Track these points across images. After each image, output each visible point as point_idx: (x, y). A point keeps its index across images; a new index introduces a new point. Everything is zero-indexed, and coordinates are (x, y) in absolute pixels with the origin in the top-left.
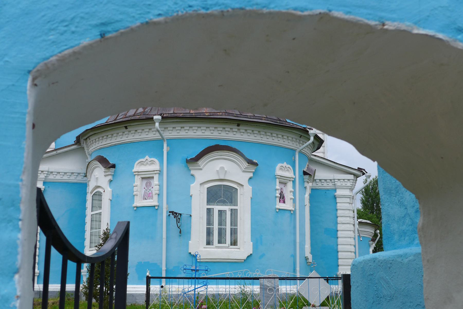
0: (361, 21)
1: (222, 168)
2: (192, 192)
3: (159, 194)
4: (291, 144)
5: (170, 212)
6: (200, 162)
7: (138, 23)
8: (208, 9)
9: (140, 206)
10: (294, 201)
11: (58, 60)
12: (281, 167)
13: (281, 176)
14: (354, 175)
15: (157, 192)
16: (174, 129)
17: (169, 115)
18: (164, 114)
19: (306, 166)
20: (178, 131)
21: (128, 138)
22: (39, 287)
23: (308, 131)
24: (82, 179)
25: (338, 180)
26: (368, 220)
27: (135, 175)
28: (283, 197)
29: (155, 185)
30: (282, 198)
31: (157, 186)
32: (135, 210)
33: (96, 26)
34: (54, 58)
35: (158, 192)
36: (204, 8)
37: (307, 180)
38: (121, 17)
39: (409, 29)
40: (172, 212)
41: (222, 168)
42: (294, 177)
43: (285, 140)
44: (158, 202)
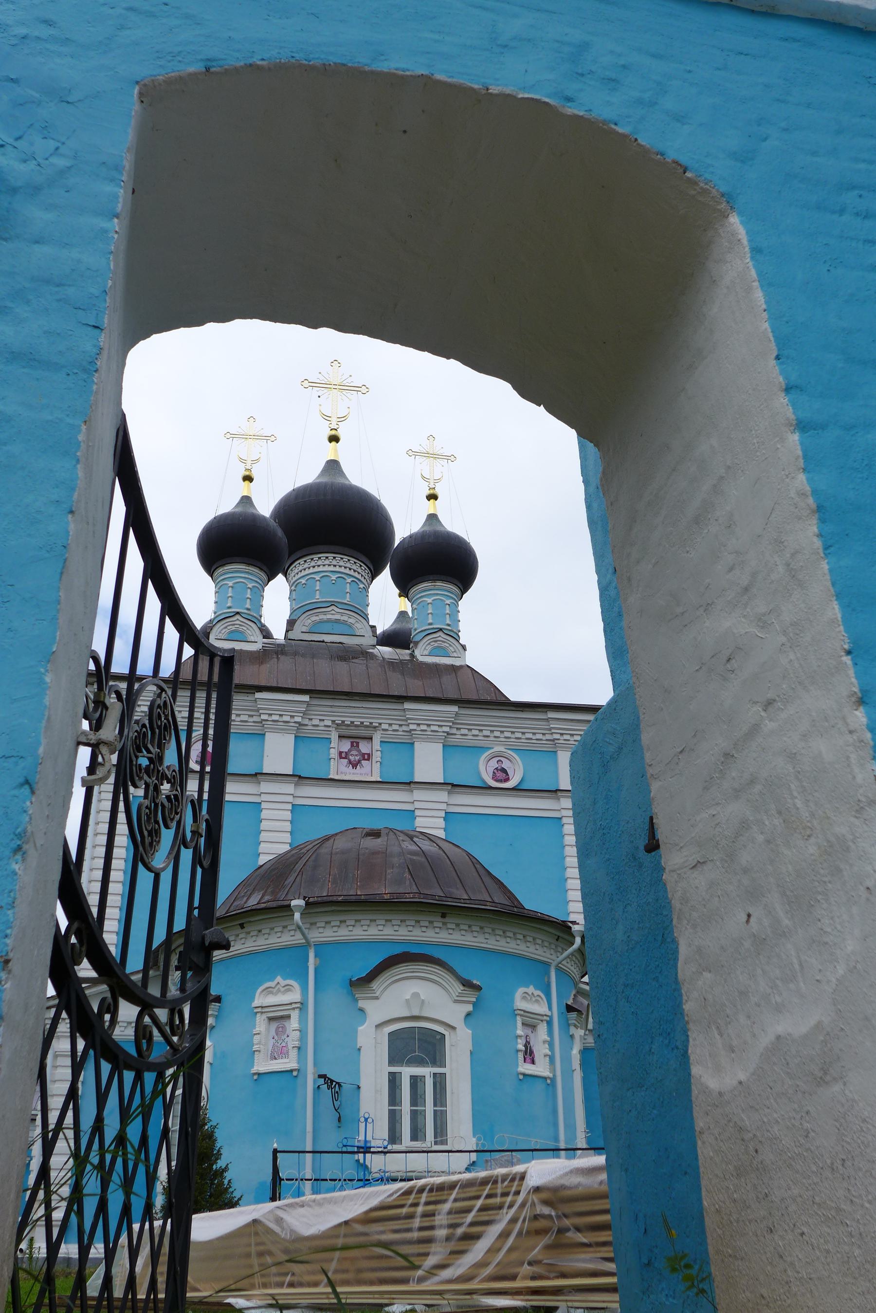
0: (464, 84)
1: (416, 995)
2: (361, 1041)
3: (299, 1048)
4: (540, 952)
5: (320, 1076)
6: (375, 985)
7: (242, 63)
8: (310, 61)
9: (264, 1071)
10: (552, 1059)
11: (164, 81)
12: (523, 995)
13: (525, 1011)
15: (297, 1043)
16: (328, 925)
17: (319, 899)
18: (309, 898)
19: (570, 996)
20: (335, 929)
21: (246, 946)
22: (67, 1249)
23: (570, 928)
27: (256, 1013)
28: (532, 1053)
29: (293, 1030)
30: (529, 1055)
31: (297, 1031)
32: (256, 1080)
33: (202, 60)
34: (161, 77)
35: (297, 1043)
36: (306, 60)
37: (574, 1022)
38: (224, 57)
39: (514, 93)
41: (416, 995)
42: (550, 1015)
43: (528, 944)
44: (298, 1063)
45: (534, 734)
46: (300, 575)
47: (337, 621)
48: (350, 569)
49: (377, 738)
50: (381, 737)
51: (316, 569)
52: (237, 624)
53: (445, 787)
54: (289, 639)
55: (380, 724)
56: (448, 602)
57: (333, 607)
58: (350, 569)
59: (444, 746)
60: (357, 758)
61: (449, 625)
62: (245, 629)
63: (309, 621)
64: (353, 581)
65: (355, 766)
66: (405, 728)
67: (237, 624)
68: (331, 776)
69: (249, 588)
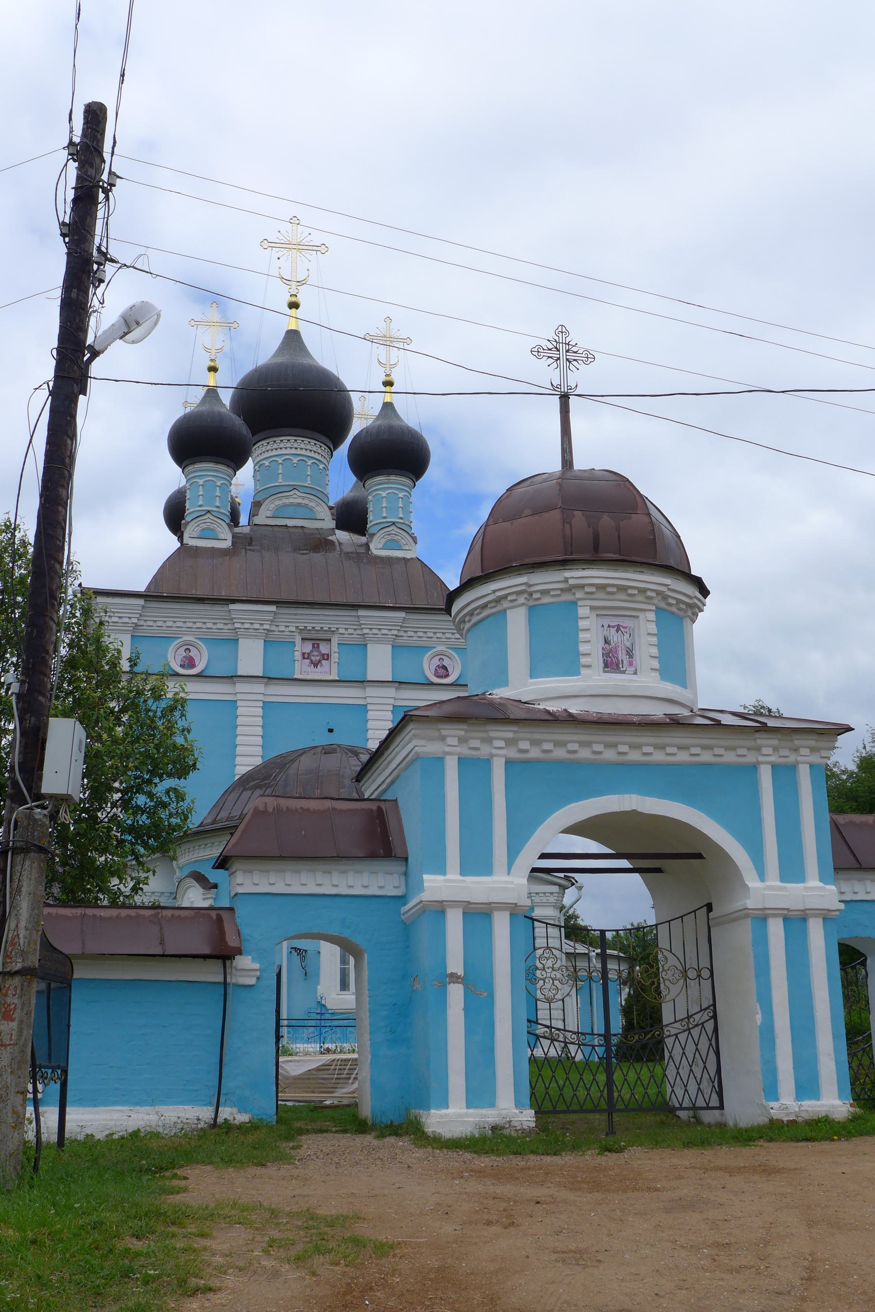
5: (292, 948)
14: (560, 885)
24: (167, 901)
25: (536, 893)
26: (614, 950)
40: (295, 948)
45: (214, 624)
46: (264, 456)
47: (299, 505)
48: (311, 451)
49: (335, 641)
50: (339, 640)
51: (279, 452)
52: (208, 522)
53: (393, 684)
54: (255, 525)
55: (337, 628)
56: (401, 495)
57: (295, 491)
58: (311, 451)
59: (393, 646)
60: (318, 658)
61: (401, 518)
62: (216, 526)
63: (273, 506)
64: (314, 463)
65: (316, 665)
66: (358, 632)
67: (208, 522)
68: (295, 677)
69: (218, 486)
